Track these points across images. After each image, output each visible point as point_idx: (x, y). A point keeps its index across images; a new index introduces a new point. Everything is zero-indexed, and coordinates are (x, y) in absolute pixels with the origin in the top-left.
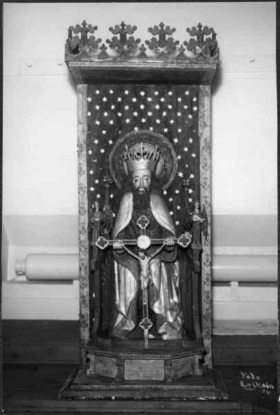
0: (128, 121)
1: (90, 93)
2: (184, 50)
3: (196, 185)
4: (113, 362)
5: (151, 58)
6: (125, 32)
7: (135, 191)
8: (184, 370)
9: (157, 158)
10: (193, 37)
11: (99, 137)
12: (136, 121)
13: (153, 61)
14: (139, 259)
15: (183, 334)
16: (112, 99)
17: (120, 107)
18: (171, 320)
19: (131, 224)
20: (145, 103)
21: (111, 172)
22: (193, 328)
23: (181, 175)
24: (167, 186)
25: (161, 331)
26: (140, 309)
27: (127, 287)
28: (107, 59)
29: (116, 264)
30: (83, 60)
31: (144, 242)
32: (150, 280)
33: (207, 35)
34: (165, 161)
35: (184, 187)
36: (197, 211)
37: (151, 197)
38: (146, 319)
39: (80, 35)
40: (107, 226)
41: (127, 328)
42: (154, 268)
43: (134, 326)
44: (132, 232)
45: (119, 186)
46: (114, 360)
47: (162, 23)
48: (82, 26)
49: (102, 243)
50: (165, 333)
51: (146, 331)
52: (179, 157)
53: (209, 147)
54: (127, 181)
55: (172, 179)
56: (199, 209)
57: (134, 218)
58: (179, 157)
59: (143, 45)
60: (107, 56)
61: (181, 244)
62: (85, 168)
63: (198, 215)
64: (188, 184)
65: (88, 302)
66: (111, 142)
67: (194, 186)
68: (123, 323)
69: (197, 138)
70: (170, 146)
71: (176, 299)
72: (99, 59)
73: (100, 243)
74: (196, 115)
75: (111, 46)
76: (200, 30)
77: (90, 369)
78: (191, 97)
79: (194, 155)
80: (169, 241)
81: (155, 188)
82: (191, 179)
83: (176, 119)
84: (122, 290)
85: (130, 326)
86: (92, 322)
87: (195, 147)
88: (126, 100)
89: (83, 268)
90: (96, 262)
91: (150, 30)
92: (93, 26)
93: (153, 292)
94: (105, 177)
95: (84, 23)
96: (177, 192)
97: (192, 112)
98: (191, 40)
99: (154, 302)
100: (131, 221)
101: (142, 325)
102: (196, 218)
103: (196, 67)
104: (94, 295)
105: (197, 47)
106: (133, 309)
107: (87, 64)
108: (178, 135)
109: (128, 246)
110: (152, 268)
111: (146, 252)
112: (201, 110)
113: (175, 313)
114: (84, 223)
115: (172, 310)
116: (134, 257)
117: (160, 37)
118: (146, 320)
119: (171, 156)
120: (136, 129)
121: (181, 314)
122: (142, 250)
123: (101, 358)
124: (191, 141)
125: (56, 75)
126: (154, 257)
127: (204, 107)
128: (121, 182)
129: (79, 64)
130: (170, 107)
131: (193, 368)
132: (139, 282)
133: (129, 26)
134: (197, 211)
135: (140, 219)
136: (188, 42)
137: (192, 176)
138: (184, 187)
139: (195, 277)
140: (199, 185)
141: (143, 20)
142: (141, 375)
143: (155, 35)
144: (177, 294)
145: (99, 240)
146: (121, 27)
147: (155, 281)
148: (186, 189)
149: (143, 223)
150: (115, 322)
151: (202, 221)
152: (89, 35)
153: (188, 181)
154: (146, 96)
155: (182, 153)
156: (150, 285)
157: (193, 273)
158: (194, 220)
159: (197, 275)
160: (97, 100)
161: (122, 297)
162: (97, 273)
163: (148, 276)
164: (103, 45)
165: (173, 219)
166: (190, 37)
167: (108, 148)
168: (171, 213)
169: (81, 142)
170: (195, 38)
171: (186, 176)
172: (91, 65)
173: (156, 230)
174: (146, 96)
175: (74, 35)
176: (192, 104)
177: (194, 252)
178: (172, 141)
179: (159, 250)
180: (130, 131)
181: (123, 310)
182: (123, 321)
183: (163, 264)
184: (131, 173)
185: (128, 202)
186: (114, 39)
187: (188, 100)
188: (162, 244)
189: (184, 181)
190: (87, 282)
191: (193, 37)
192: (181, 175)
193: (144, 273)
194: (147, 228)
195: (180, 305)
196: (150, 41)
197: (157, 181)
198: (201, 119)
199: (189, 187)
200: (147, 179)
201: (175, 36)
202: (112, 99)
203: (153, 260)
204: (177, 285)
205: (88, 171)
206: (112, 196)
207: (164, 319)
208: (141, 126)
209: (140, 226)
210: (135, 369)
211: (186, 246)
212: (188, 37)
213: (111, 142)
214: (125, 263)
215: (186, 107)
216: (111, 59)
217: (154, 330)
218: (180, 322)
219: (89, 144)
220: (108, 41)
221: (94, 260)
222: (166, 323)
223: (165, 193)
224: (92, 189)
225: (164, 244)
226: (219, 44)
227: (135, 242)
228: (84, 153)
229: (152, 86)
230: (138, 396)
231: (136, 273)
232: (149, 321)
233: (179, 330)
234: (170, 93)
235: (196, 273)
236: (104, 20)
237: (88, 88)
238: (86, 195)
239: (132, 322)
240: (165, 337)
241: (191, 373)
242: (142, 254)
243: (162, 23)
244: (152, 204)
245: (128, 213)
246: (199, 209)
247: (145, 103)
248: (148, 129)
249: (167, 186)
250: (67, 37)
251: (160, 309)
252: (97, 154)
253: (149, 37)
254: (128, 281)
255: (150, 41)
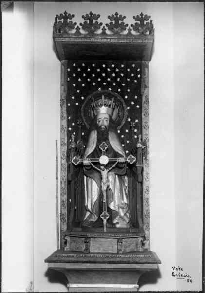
0: (94, 84)
1: (69, 65)
2: (131, 30)
3: (139, 127)
4: (83, 241)
5: (109, 35)
6: (92, 18)
7: (98, 128)
8: (131, 248)
9: (113, 107)
10: (137, 22)
11: (75, 94)
12: (99, 85)
13: (110, 38)
14: (101, 171)
15: (130, 225)
16: (84, 70)
17: (89, 75)
18: (122, 214)
19: (95, 150)
20: (106, 72)
21: (83, 118)
22: (137, 222)
23: (129, 120)
24: (120, 127)
25: (115, 221)
26: (101, 205)
27: (93, 191)
28: (80, 36)
29: (85, 177)
30: (64, 36)
31: (104, 160)
32: (108, 186)
33: (146, 20)
34: (119, 111)
35: (131, 127)
36: (140, 141)
37: (109, 133)
38: (105, 213)
39: (62, 20)
40: (80, 152)
41: (92, 220)
42: (111, 178)
43: (97, 218)
44: (97, 153)
45: (88, 127)
46: (83, 239)
47: (116, 13)
48: (64, 15)
49: (76, 161)
50: (118, 223)
51: (105, 221)
52: (128, 108)
53: (148, 101)
54: (93, 123)
55: (123, 122)
56: (142, 139)
57: (97, 146)
58: (128, 108)
59: (104, 27)
60: (80, 34)
61: (129, 161)
62: (65, 115)
63: (140, 143)
64: (134, 125)
65: (66, 205)
66: (83, 98)
67: (138, 127)
68: (90, 217)
69: (140, 96)
70: (122, 100)
71: (125, 201)
72: (75, 35)
73: (75, 160)
74: (139, 80)
75: (83, 28)
76: (142, 17)
77: (67, 247)
78: (136, 68)
79: (138, 107)
80: (122, 160)
81: (113, 128)
82: (136, 123)
83: (126, 82)
84: (89, 194)
85: (94, 218)
86: (68, 219)
87: (139, 102)
88: (93, 70)
89: (63, 182)
90: (72, 175)
91: (109, 17)
92: (71, 14)
93: (110, 195)
94: (78, 120)
95: (66, 13)
96: (127, 131)
97: (136, 78)
98: (136, 24)
99: (111, 202)
100: (95, 149)
101: (102, 216)
102: (139, 145)
103: (139, 41)
104: (70, 200)
105: (140, 28)
106: (97, 207)
107: (67, 39)
108: (127, 94)
109: (93, 163)
110: (111, 180)
111: (106, 166)
112: (143, 77)
113: (125, 210)
114: (64, 152)
115: (123, 208)
116: (97, 170)
117: (115, 22)
118: (105, 213)
119: (123, 107)
120: (100, 89)
121: (129, 212)
122: (103, 165)
123: (75, 239)
124: (136, 97)
125: (33, 156)
126: (112, 170)
127: (145, 75)
128: (89, 124)
129: (61, 39)
130: (122, 75)
131: (137, 247)
132: (101, 187)
133: (95, 15)
134: (140, 141)
135: (101, 145)
136: (134, 25)
137: (137, 121)
138: (131, 127)
139: (139, 185)
140: (141, 126)
141: (104, 13)
142: (102, 249)
143: (112, 20)
144: (127, 197)
145: (74, 158)
146: (89, 15)
147: (111, 187)
148: (133, 129)
149: (103, 147)
150: (84, 217)
151: (143, 148)
152: (69, 20)
153: (134, 123)
154: (107, 67)
155: (130, 105)
156: (108, 189)
157: (137, 183)
158: (138, 146)
159: (140, 184)
160: (74, 70)
161: (89, 199)
162: (73, 182)
163: (107, 182)
164: (78, 27)
165: (124, 149)
166: (135, 22)
167: (81, 102)
168: (123, 145)
169: (63, 98)
170: (139, 22)
171: (133, 120)
172: (69, 40)
173: (110, 151)
174: (107, 67)
175: (58, 20)
176: (137, 73)
177: (138, 168)
178: (123, 97)
179: (114, 165)
180: (95, 91)
181: (89, 207)
182: (90, 217)
183: (117, 176)
184: (96, 117)
185: (94, 136)
186: (85, 23)
187: (134, 70)
188: (115, 162)
189: (132, 123)
190: (66, 191)
191: (137, 22)
192: (129, 120)
193: (104, 180)
194: (106, 151)
195: (128, 205)
196: (109, 24)
197: (113, 124)
198: (144, 83)
199: (135, 128)
200: (107, 121)
201: (125, 21)
202: (84, 70)
203: (110, 173)
204: (127, 192)
205: (68, 117)
206: (83, 134)
207: (117, 213)
208: (103, 87)
209: (102, 149)
210: (98, 245)
211: (130, 156)
212: (134, 22)
213: (83, 98)
214: (90, 176)
215: (133, 75)
216: (83, 36)
217: (110, 220)
218: (128, 217)
219: (68, 99)
220: (81, 24)
221: (70, 174)
222: (119, 217)
223: (119, 132)
224: (70, 129)
225: (118, 161)
226: (154, 26)
227: (98, 160)
228: (65, 105)
229: (110, 61)
230: (99, 260)
231: (99, 182)
232: (107, 214)
233: (127, 221)
234: (122, 66)
235: (139, 182)
236: (78, 14)
237: (68, 62)
238: (66, 133)
239: (96, 216)
240: (118, 226)
241: (136, 250)
242: (102, 167)
243: (116, 13)
244: (110, 138)
245: (94, 143)
246: (142, 139)
247: (106, 72)
248: (108, 89)
249: (120, 127)
250: (55, 21)
251: (115, 207)
252: (73, 105)
253: (108, 21)
254: (93, 187)
255: (109, 24)
